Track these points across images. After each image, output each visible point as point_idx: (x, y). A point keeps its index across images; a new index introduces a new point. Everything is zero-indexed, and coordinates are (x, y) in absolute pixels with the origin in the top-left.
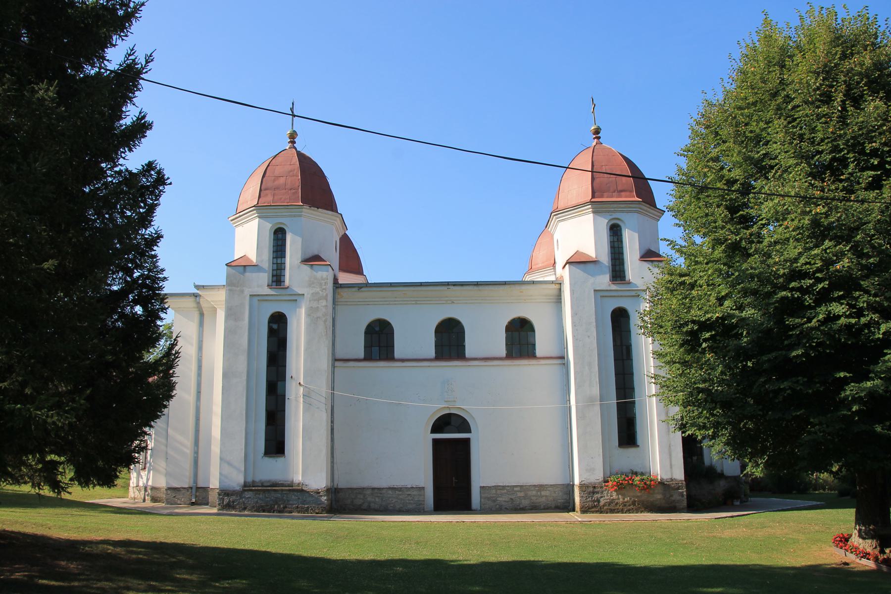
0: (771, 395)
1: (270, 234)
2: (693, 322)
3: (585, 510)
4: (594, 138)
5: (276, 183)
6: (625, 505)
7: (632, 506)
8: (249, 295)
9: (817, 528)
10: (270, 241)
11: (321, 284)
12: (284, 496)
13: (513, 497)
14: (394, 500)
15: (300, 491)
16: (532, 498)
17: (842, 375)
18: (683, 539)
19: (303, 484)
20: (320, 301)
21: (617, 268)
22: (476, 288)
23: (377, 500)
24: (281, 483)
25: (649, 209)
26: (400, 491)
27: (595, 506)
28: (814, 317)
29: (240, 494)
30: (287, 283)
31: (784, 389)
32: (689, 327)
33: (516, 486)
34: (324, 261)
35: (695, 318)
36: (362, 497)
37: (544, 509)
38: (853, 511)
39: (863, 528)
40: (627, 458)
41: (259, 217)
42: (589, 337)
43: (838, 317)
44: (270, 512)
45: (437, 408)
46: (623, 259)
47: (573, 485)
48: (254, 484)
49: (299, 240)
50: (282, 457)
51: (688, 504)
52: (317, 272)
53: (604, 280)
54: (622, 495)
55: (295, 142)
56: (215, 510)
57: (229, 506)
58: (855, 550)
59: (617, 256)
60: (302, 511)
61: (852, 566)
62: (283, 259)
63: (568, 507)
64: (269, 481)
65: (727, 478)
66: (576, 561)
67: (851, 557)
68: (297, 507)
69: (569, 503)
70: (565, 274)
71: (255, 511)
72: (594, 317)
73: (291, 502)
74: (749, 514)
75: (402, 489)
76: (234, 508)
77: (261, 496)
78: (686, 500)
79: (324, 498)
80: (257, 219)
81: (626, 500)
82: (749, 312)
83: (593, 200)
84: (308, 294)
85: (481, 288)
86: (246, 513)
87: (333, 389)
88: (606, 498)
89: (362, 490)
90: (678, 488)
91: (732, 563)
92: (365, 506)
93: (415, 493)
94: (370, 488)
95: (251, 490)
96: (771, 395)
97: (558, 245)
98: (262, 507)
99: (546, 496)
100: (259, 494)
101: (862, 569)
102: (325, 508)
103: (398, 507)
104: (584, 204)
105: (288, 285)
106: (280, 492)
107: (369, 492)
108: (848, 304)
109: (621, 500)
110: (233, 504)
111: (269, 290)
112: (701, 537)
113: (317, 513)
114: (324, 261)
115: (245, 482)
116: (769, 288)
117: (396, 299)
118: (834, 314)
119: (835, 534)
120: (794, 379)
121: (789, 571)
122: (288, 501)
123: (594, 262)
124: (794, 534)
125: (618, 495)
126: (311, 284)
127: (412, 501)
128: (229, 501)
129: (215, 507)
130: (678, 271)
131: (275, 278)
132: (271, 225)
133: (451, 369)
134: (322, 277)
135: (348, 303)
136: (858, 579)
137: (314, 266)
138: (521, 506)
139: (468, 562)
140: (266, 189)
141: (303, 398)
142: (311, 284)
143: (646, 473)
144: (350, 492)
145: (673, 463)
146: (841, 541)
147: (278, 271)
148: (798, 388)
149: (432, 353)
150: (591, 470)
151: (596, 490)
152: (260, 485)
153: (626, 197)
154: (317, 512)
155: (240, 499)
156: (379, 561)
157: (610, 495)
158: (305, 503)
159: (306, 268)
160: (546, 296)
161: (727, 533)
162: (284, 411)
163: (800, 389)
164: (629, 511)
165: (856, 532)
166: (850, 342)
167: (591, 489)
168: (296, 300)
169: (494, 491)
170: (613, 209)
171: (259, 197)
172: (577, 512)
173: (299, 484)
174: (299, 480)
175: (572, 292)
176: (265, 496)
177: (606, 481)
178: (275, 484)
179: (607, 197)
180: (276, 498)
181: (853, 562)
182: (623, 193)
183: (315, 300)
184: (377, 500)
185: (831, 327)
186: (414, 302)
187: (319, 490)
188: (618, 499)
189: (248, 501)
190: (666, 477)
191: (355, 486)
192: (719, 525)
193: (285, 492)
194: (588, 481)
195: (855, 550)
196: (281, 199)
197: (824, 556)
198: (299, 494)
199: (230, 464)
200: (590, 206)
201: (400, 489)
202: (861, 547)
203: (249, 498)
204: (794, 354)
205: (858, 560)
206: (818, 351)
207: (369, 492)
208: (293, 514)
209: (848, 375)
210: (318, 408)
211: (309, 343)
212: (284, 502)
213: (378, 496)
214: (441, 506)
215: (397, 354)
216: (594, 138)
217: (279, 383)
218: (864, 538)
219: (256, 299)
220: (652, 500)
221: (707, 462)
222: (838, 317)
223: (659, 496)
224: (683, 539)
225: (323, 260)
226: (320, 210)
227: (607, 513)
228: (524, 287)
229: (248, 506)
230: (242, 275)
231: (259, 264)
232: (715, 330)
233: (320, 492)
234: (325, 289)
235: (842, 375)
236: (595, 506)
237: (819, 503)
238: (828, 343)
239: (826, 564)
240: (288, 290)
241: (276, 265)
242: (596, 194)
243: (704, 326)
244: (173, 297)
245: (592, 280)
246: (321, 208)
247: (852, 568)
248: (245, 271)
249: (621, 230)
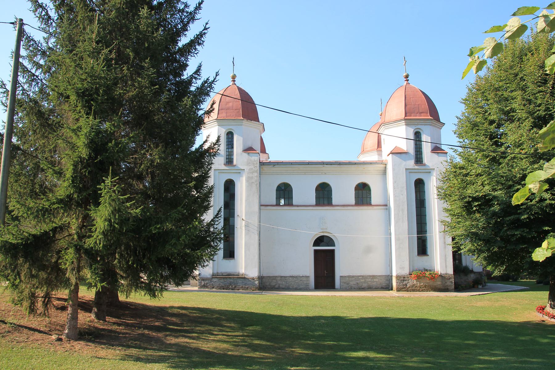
0: (510, 237)
1: (225, 135)
2: (469, 197)
3: (399, 290)
4: (405, 81)
5: (227, 106)
6: (421, 288)
7: (424, 288)
9: (526, 302)
10: (224, 139)
11: (254, 164)
13: (358, 282)
14: (293, 283)
15: (244, 278)
16: (369, 283)
17: (547, 228)
18: (457, 307)
19: (245, 274)
21: (418, 156)
22: (339, 166)
25: (437, 123)
27: (404, 288)
28: (534, 199)
29: (210, 279)
31: (517, 235)
32: (467, 199)
33: (360, 276)
34: (255, 150)
35: (470, 195)
36: (275, 281)
37: (375, 289)
38: (547, 293)
39: (553, 303)
40: (422, 262)
41: (219, 125)
42: (402, 195)
43: (546, 200)
45: (318, 233)
46: (422, 152)
47: (392, 276)
51: (455, 287)
52: (251, 157)
53: (411, 163)
54: (419, 282)
55: (235, 81)
56: (196, 288)
57: (204, 286)
58: (548, 314)
59: (418, 150)
61: (546, 322)
62: (232, 149)
63: (389, 287)
64: (226, 273)
65: (475, 273)
66: (407, 317)
67: (546, 318)
68: (242, 287)
69: (389, 286)
70: (390, 160)
71: (219, 289)
72: (405, 183)
73: (239, 284)
74: (488, 293)
76: (207, 287)
77: (222, 281)
78: (454, 285)
79: (257, 282)
80: (217, 127)
81: (421, 284)
82: (498, 193)
83: (406, 118)
85: (341, 166)
86: (214, 290)
87: (260, 222)
88: (410, 283)
89: (275, 278)
90: (450, 279)
91: (485, 320)
92: (277, 286)
93: (305, 279)
96: (510, 237)
97: (384, 141)
98: (223, 286)
99: (376, 282)
101: (552, 324)
103: (295, 287)
104: (401, 120)
108: (551, 193)
109: (419, 284)
111: (225, 167)
112: (466, 306)
113: (253, 290)
114: (255, 150)
116: (511, 183)
117: (294, 172)
118: (544, 198)
119: (537, 305)
120: (522, 230)
121: (515, 324)
122: (237, 283)
123: (406, 153)
124: (515, 305)
125: (417, 282)
126: (248, 164)
127: (303, 284)
128: (205, 284)
129: (197, 286)
130: (458, 166)
131: (228, 160)
133: (324, 211)
134: (254, 160)
136: (550, 328)
137: (250, 154)
138: (363, 287)
139: (352, 318)
140: (222, 109)
142: (248, 164)
143: (432, 270)
145: (447, 265)
146: (540, 309)
148: (524, 235)
149: (313, 202)
150: (403, 268)
151: (405, 279)
152: (221, 275)
153: (424, 116)
155: (210, 282)
156: (310, 317)
157: (412, 282)
159: (245, 155)
160: (378, 171)
161: (479, 304)
162: (233, 234)
163: (525, 235)
164: (423, 291)
165: (549, 305)
166: (551, 213)
167: (402, 279)
169: (348, 279)
170: (416, 123)
171: (218, 114)
172: (394, 291)
173: (243, 274)
175: (394, 170)
177: (410, 274)
178: (229, 275)
179: (413, 116)
181: (547, 320)
182: (422, 114)
183: (251, 173)
184: (283, 283)
185: (542, 205)
188: (417, 284)
190: (443, 272)
191: (271, 275)
192: (474, 299)
194: (401, 274)
195: (548, 314)
196: (230, 115)
197: (532, 317)
200: (404, 121)
201: (296, 277)
202: (551, 313)
203: (216, 282)
204: (523, 217)
205: (549, 319)
206: (535, 216)
207: (279, 278)
209: (550, 229)
210: (253, 233)
211: (248, 197)
214: (319, 286)
216: (405, 81)
217: (231, 219)
218: (553, 308)
220: (435, 285)
221: (464, 264)
222: (546, 200)
223: (439, 283)
224: (457, 307)
227: (411, 292)
228: (365, 166)
232: (480, 201)
234: (256, 167)
235: (547, 228)
236: (404, 288)
237: (526, 288)
238: (540, 213)
239: (533, 321)
240: (235, 167)
242: (407, 114)
243: (475, 199)
245: (404, 163)
247: (547, 323)
249: (421, 135)
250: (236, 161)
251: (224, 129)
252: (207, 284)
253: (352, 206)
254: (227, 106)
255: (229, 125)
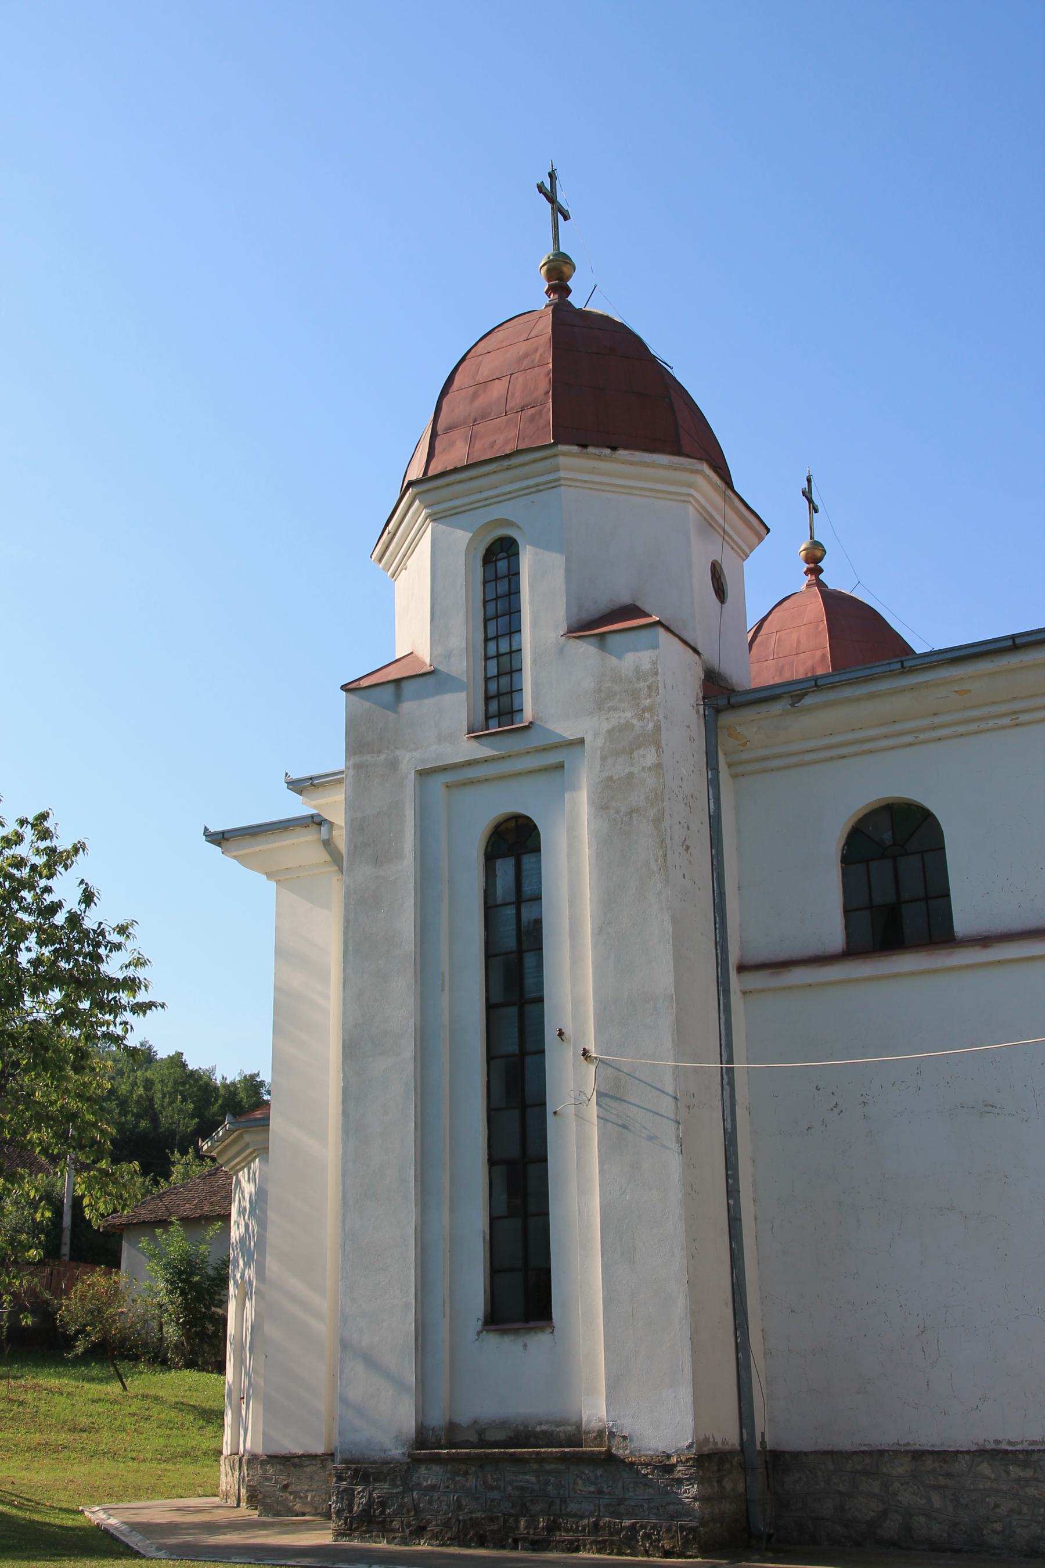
5: (479, 402)
8: (412, 776)
11: (634, 696)
12: (547, 1483)
19: (612, 1435)
20: (635, 754)
23: (936, 1501)
24: (544, 1432)
26: (1025, 1465)
30: (528, 715)
41: (434, 518)
44: (503, 1547)
48: (452, 1434)
49: (556, 561)
50: (542, 1329)
52: (620, 657)
60: (612, 1543)
64: (503, 1424)
68: (596, 1525)
73: (573, 1507)
75: (1035, 1457)
79: (689, 1492)
84: (595, 735)
94: (907, 1452)
95: (437, 1460)
100: (466, 1473)
102: (693, 1530)
105: (531, 720)
106: (535, 1466)
107: (901, 1470)
110: (383, 1512)
111: (474, 744)
113: (667, 1554)
115: (421, 1429)
117: (937, 720)
122: (564, 1501)
132: (472, 535)
135: (773, 764)
137: (612, 640)
141: (598, 1104)
144: (831, 1467)
147: (504, 681)
152: (474, 1438)
154: (667, 1547)
158: (622, 1509)
159: (585, 650)
168: (560, 767)
173: (601, 1433)
174: (600, 1420)
176: (485, 1482)
180: (522, 1488)
184: (936, 1501)
186: (1006, 721)
187: (669, 1457)
189: (430, 1502)
191: (846, 1443)
193: (553, 1466)
198: (599, 1472)
199: (370, 1361)
203: (434, 1488)
208: (582, 1554)
212: (551, 1504)
213: (937, 1488)
215: (963, 922)
219: (438, 783)
225: (641, 613)
226: (622, 453)
229: (429, 1522)
230: (389, 713)
231: (440, 668)
233: (674, 1466)
234: (650, 709)
240: (532, 732)
241: (495, 661)
244: (260, 838)
246: (626, 448)
248: (398, 697)
250: (536, 699)
251: (460, 533)
252: (383, 1504)
253: (815, 684)
254: (479, 402)
255: (487, 503)
